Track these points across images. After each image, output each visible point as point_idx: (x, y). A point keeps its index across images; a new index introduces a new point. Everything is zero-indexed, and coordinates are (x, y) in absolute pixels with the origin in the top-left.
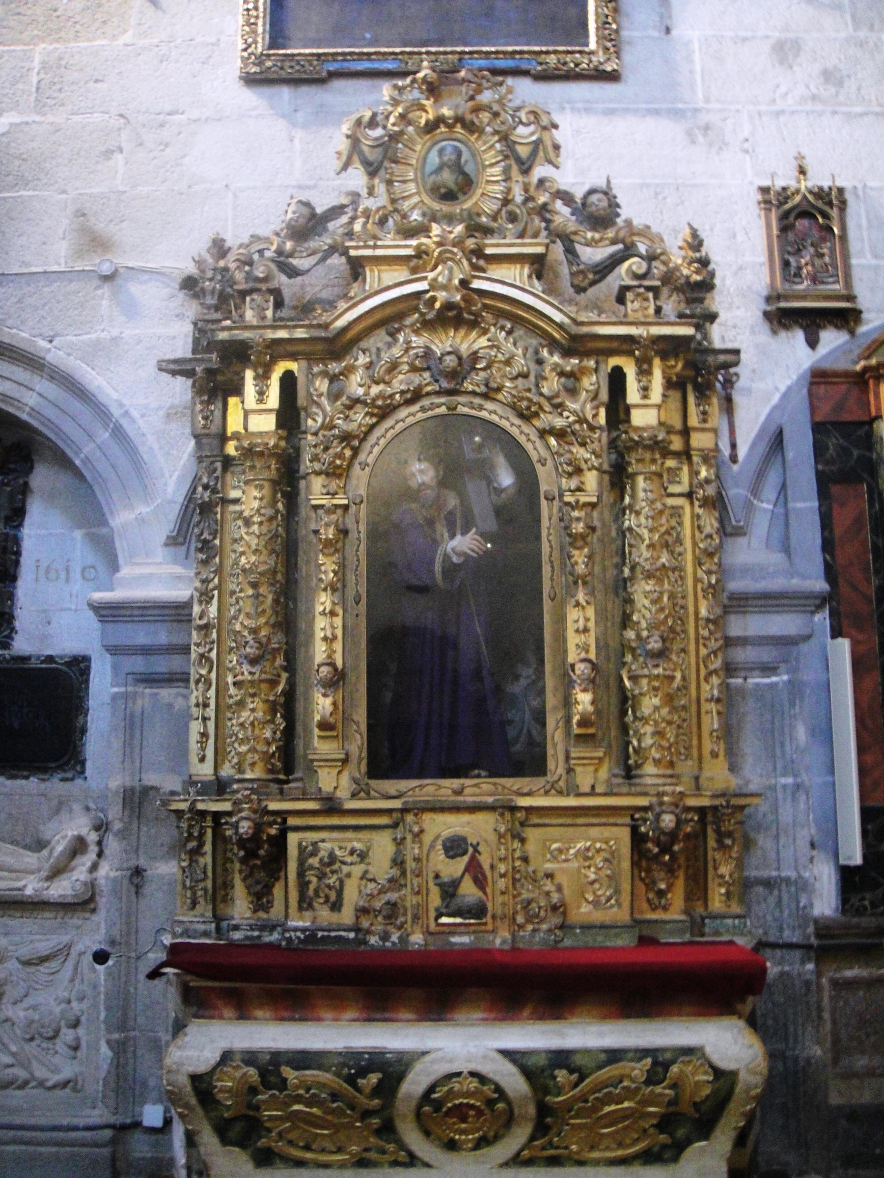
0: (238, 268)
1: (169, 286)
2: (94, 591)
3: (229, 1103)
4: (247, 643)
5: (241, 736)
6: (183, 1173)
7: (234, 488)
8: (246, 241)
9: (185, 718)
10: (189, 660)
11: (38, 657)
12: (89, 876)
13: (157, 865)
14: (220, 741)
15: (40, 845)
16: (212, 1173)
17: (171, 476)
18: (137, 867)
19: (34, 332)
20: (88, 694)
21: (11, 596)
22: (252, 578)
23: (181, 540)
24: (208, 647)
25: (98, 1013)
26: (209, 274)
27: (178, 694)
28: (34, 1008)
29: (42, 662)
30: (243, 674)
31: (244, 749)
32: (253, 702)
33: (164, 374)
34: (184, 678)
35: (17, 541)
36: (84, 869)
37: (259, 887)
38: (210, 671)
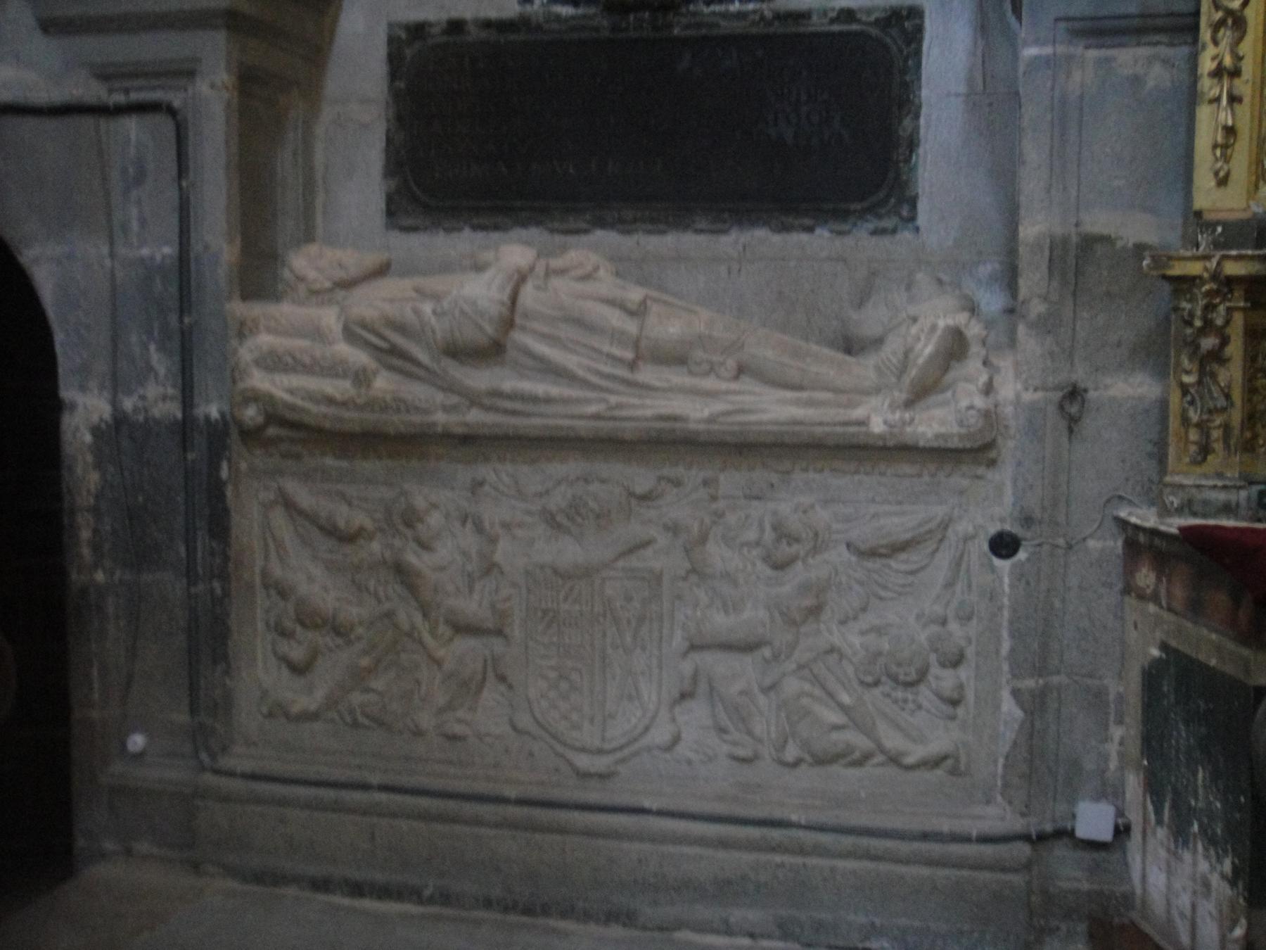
11: (825, 13)
13: (1108, 381)
20: (919, 79)
25: (999, 640)
27: (1150, 61)
28: (878, 630)
29: (832, 21)
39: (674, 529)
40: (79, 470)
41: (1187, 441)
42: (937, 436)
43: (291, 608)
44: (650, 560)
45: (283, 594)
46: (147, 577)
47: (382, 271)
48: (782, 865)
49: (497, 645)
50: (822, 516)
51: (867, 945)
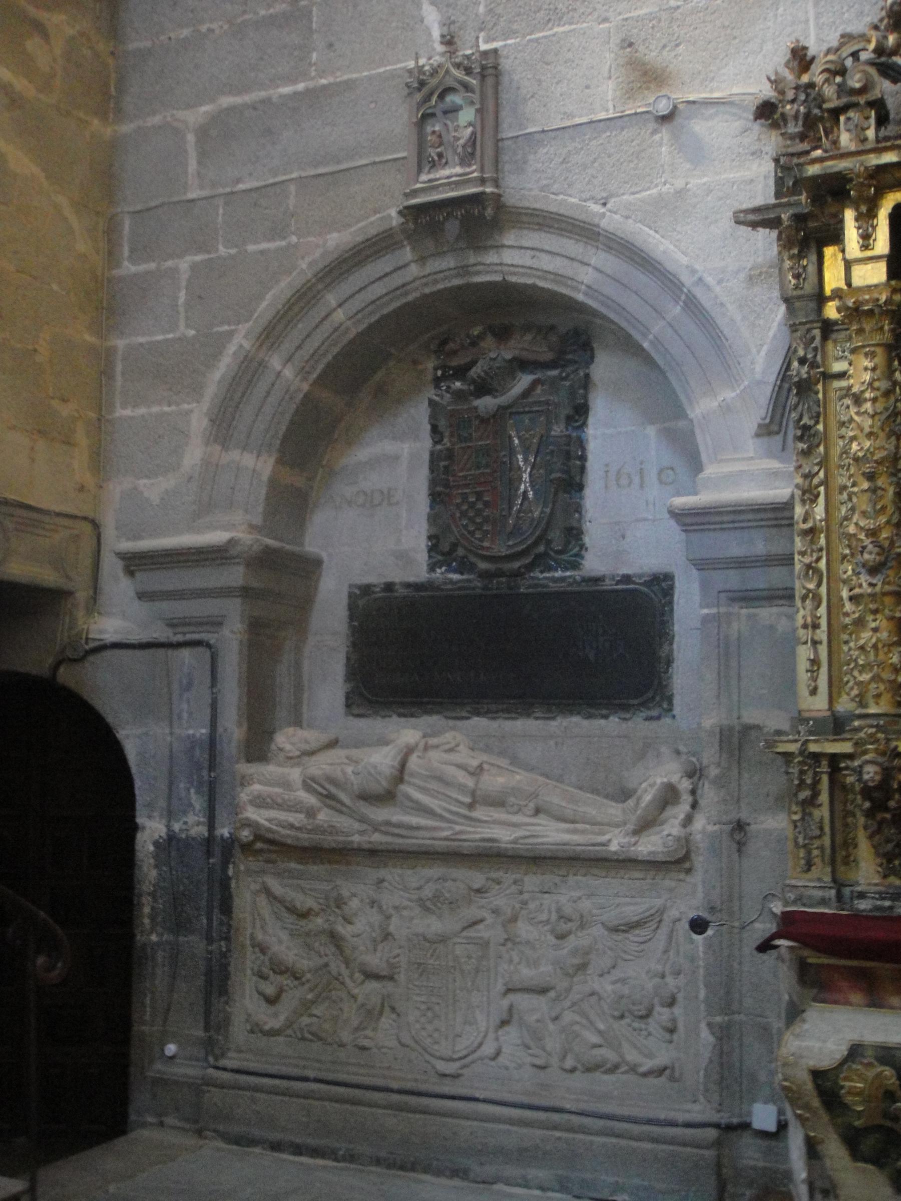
0: (827, 80)
1: (740, 118)
2: (674, 496)
3: (860, 1108)
4: (864, 548)
5: (861, 662)
6: (803, 1190)
7: (838, 359)
8: (835, 44)
9: (792, 641)
10: (792, 572)
11: (613, 578)
12: (683, 830)
13: (762, 818)
14: (835, 667)
15: (624, 794)
16: (842, 1193)
17: (759, 352)
18: (739, 821)
19: (584, 196)
20: (672, 619)
21: (579, 509)
22: (867, 468)
23: (775, 428)
24: (815, 556)
26: (790, 95)
28: (623, 981)
29: (618, 583)
30: (860, 586)
31: (865, 677)
32: (875, 620)
33: (742, 228)
34: (787, 596)
35: (581, 444)
36: (677, 822)
37: (890, 846)
38: (819, 585)
39: (496, 911)
40: (145, 869)
41: (798, 857)
42: (650, 853)
43: (267, 958)
44: (481, 932)
45: (263, 950)
46: (182, 939)
47: (333, 744)
48: (559, 1138)
49: (390, 986)
50: (586, 905)
51: (614, 1198)
